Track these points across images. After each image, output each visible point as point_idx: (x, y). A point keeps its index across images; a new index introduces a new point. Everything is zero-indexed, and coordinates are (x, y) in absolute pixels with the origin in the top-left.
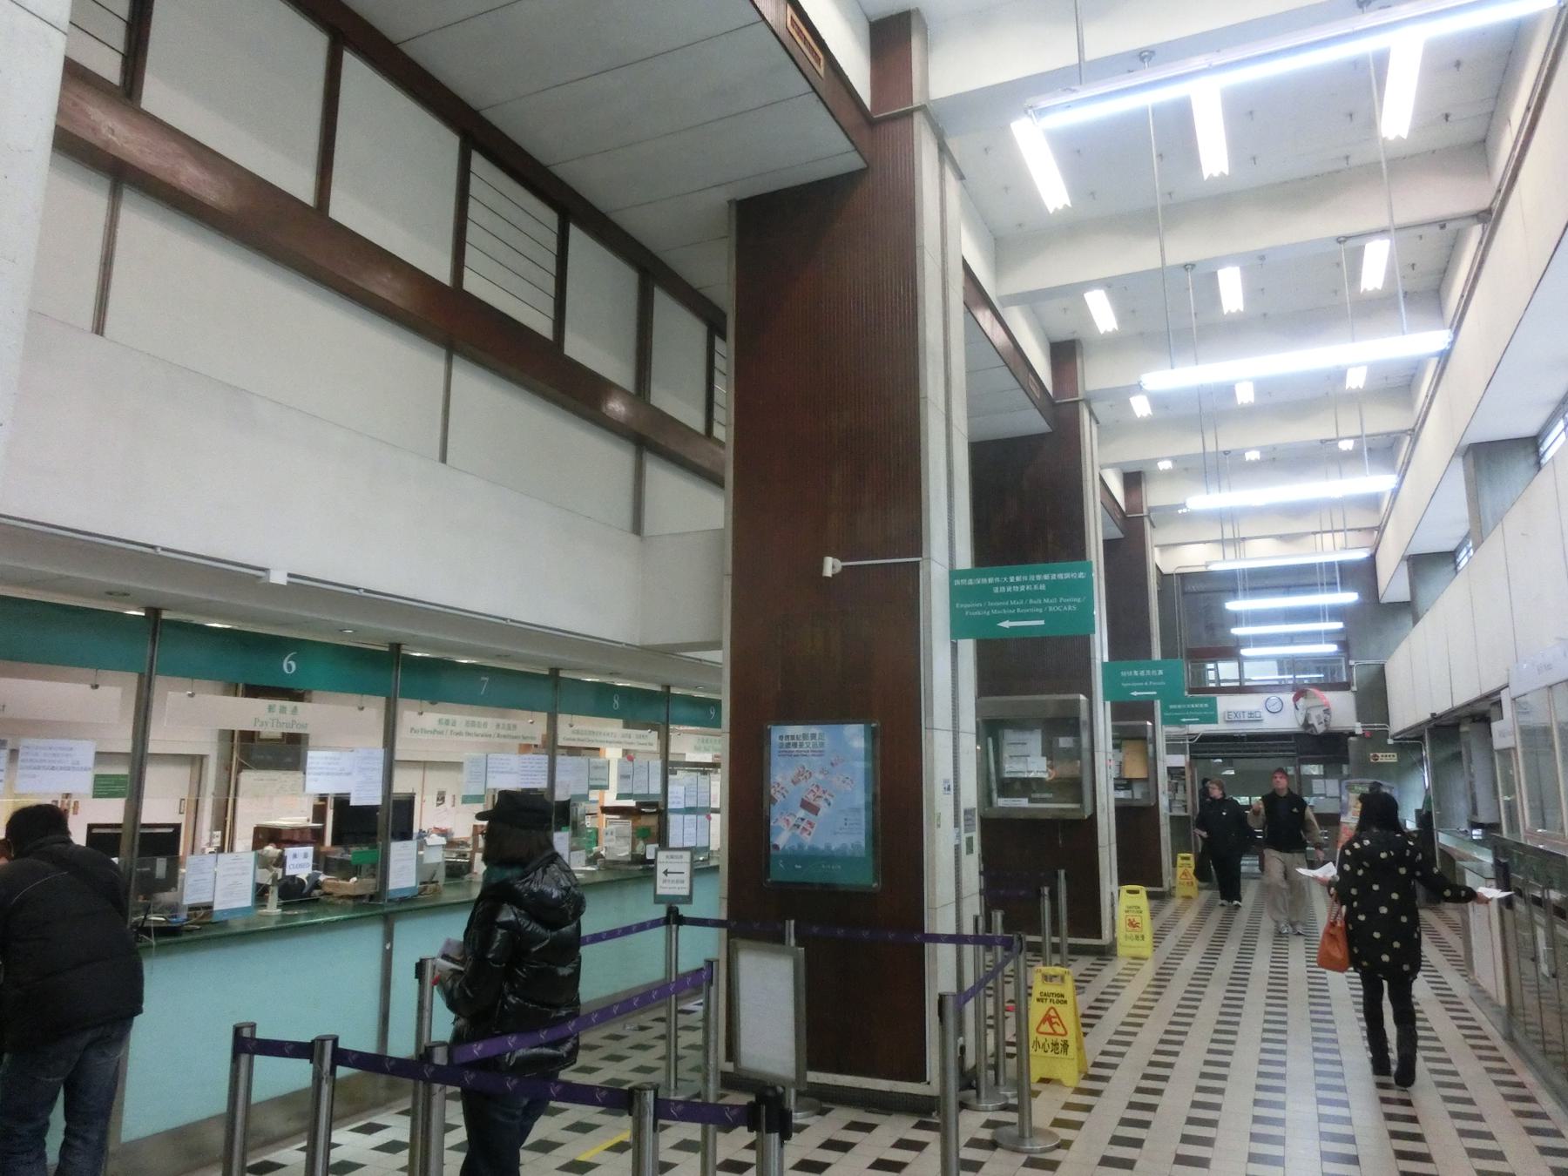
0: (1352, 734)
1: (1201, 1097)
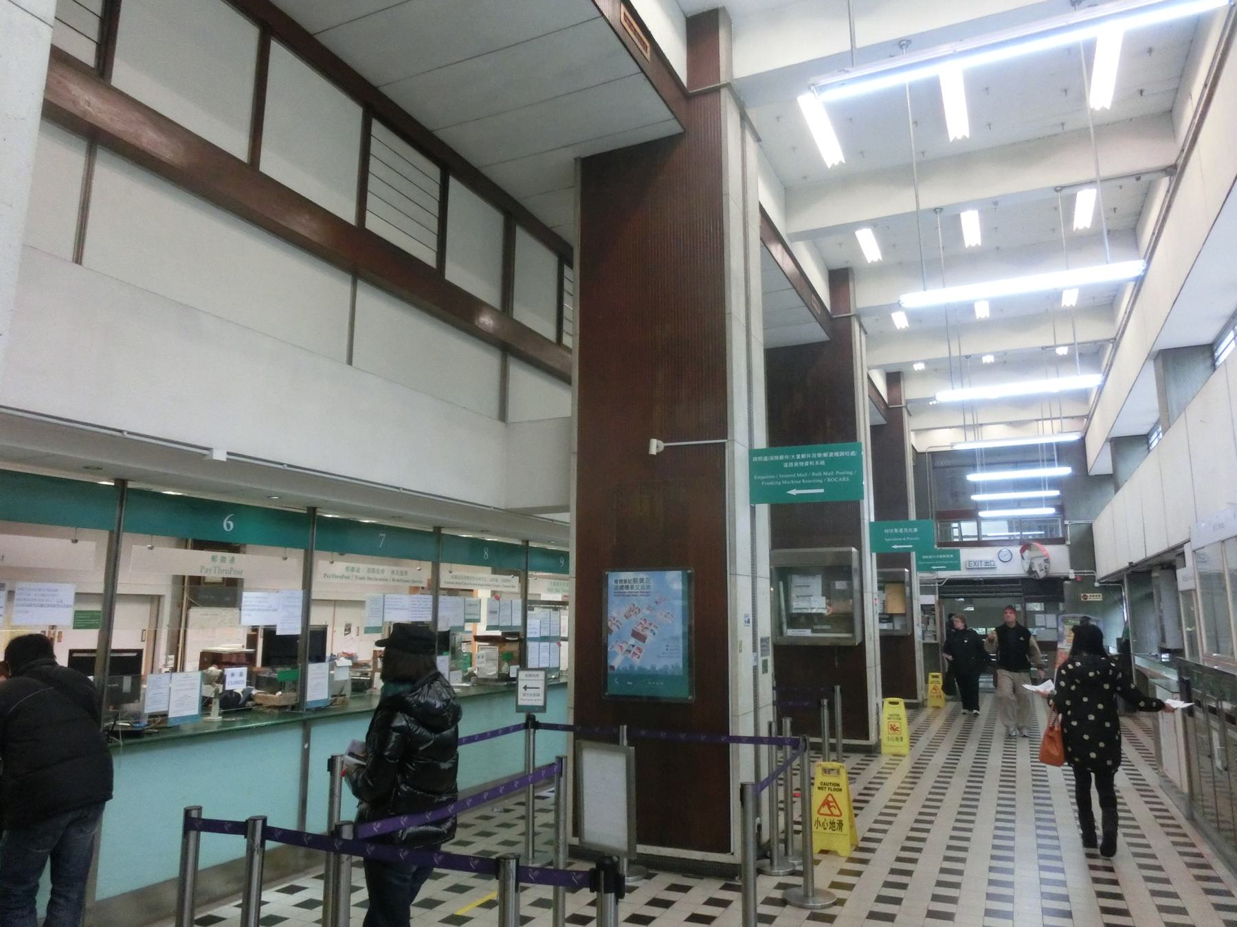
0: (1067, 578)
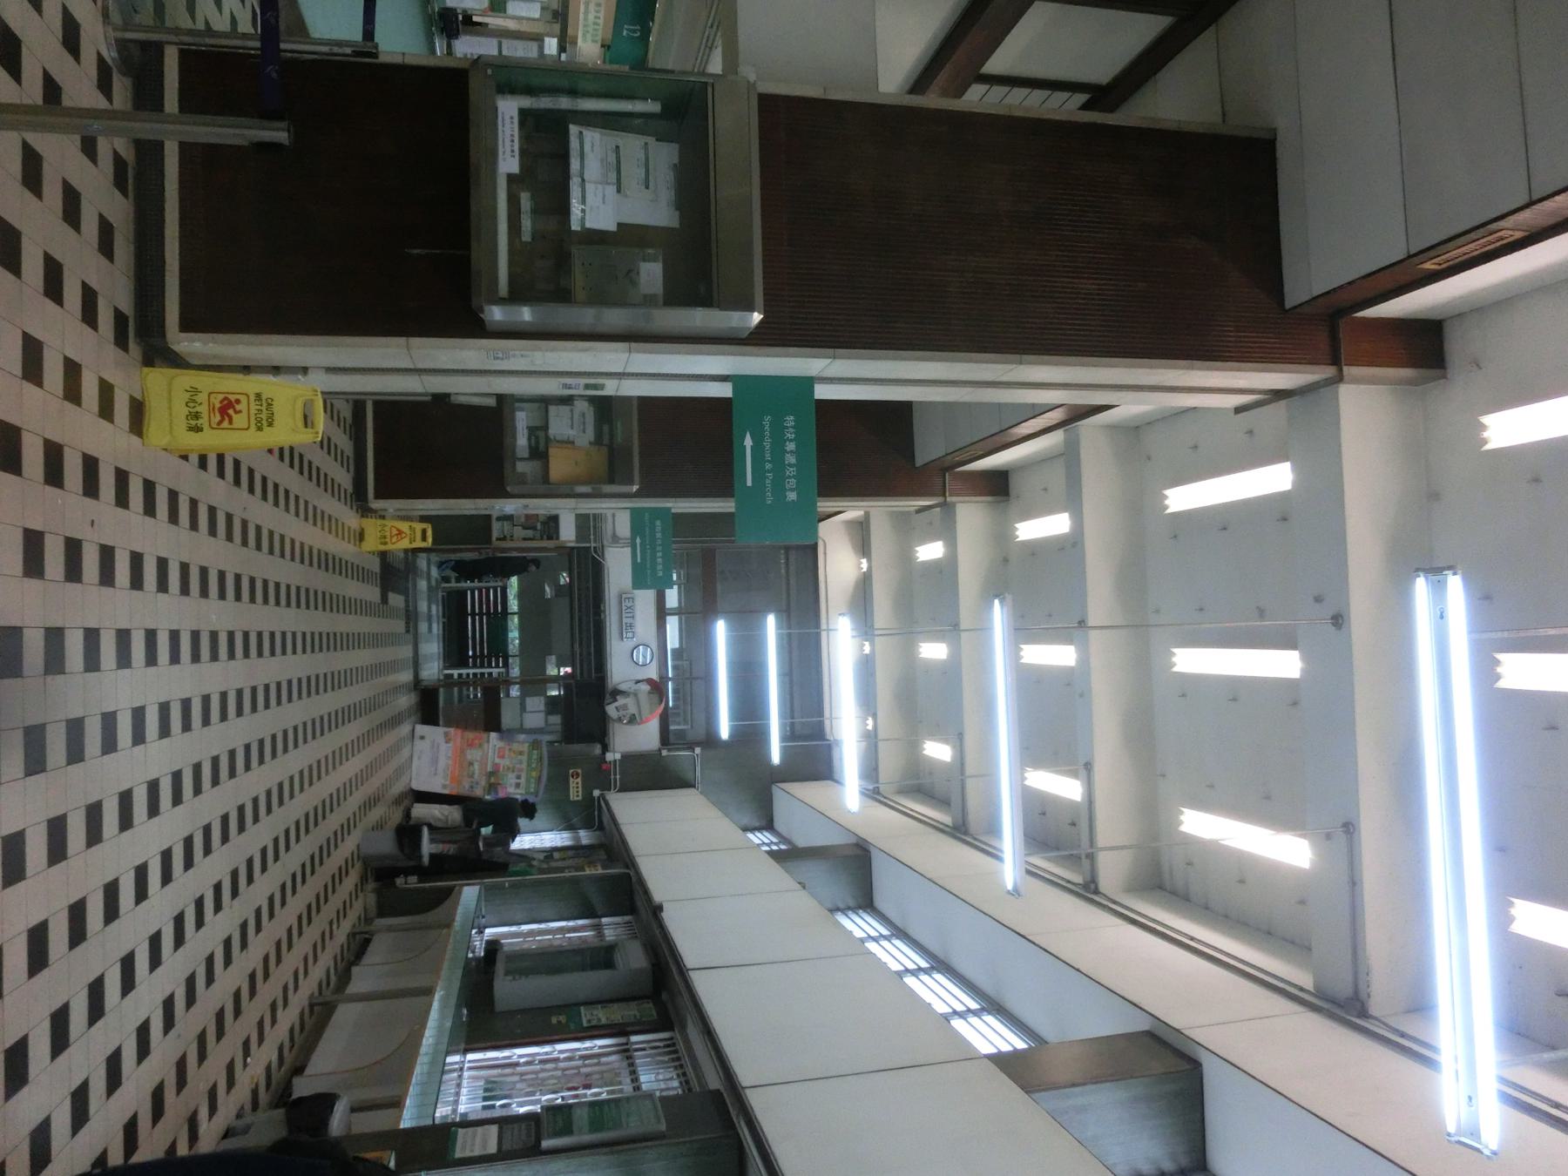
0: (605, 748)
1: (259, 585)
